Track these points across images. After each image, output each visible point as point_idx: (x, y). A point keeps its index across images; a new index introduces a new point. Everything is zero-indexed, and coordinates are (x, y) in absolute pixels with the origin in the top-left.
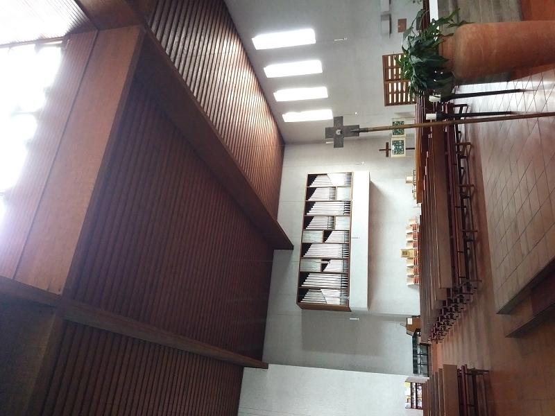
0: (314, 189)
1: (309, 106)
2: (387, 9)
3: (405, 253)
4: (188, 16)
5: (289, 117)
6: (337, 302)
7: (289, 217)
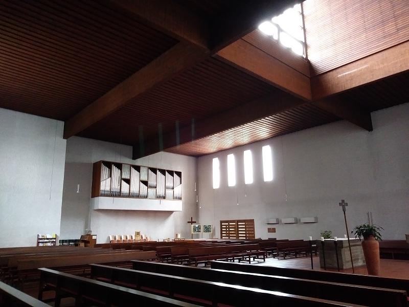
2: (302, 221)
3: (138, 234)
4: (295, 115)
5: (216, 162)
6: (102, 188)
7: (163, 159)
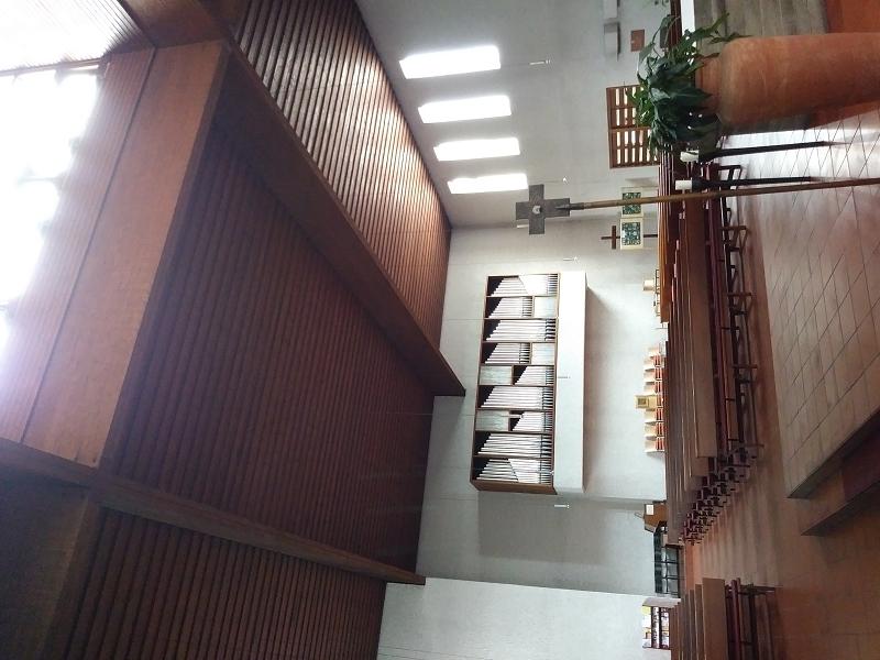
0: (498, 300)
1: (490, 168)
2: (614, 15)
3: (642, 402)
4: (298, 25)
5: (458, 186)
6: (535, 479)
7: (458, 344)
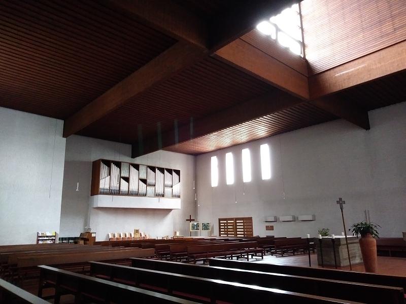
2: (299, 219)
3: (137, 231)
4: (293, 114)
5: (214, 160)
6: (101, 186)
7: (161, 157)
